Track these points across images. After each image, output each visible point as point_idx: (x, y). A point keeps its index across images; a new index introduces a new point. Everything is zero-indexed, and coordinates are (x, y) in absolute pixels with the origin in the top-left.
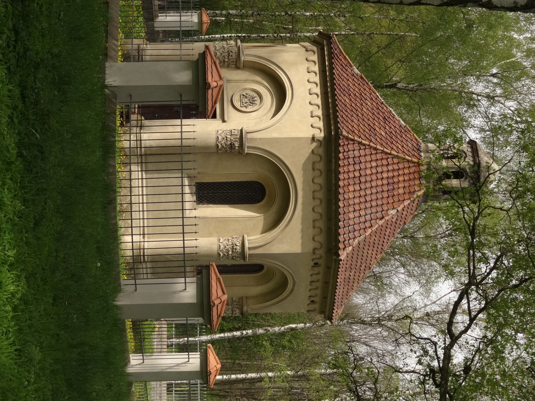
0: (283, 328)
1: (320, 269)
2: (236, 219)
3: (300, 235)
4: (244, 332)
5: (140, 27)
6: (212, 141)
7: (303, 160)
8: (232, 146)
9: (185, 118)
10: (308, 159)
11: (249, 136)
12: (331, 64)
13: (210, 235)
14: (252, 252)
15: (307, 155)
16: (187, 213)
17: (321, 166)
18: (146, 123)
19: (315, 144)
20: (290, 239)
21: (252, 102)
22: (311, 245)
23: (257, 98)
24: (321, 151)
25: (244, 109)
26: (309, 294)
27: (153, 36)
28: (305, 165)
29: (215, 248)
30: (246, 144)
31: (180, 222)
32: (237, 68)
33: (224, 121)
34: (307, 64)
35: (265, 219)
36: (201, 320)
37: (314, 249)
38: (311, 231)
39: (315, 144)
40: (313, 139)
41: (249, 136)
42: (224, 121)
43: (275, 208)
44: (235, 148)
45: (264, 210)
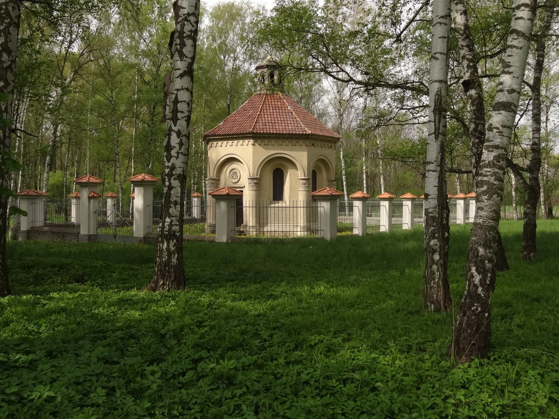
1: (315, 143)
2: (291, 182)
5: (199, 225)
6: (254, 192)
8: (256, 183)
10: (263, 147)
11: (251, 175)
12: (218, 135)
13: (298, 195)
16: (288, 205)
17: (266, 141)
18: (244, 223)
19: (256, 144)
20: (301, 157)
21: (236, 173)
23: (234, 171)
24: (259, 141)
25: (239, 177)
26: (327, 149)
27: (203, 219)
29: (304, 192)
30: (255, 177)
31: (291, 209)
32: (219, 180)
33: (244, 187)
34: (218, 147)
38: (297, 147)
39: (256, 144)
40: (253, 145)
41: (251, 175)
42: (244, 187)
43: (286, 164)
44: (257, 182)
45: (287, 169)
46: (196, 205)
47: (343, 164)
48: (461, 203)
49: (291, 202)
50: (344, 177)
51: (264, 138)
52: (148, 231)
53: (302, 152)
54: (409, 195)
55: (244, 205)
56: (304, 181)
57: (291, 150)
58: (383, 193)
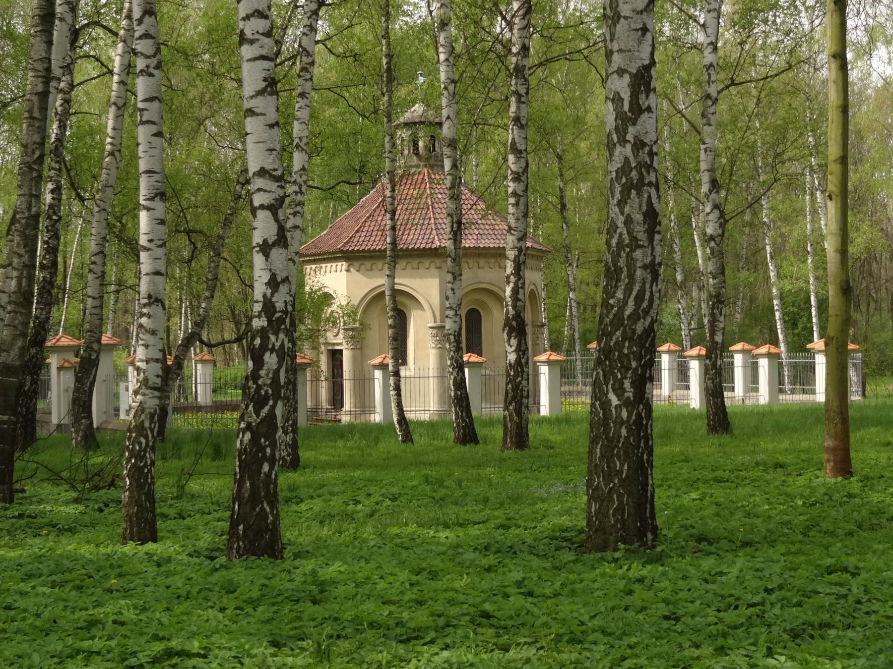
0: (771, 268)
3: (425, 280)
4: (776, 308)
7: (365, 279)
9: (342, 376)
10: (363, 274)
12: (307, 255)
14: (438, 320)
15: (360, 275)
16: (412, 374)
17: (368, 264)
19: (352, 269)
20: (426, 288)
22: (433, 270)
24: (357, 264)
28: (368, 277)
31: (413, 379)
35: (416, 309)
36: (308, 370)
37: (437, 268)
40: (348, 271)
46: (667, 367)
47: (772, 274)
48: (738, 359)
49: (417, 370)
50: (775, 302)
51: (364, 258)
52: (104, 418)
53: (430, 280)
54: (739, 346)
55: (824, 366)
56: (435, 331)
57: (411, 277)
58: (816, 340)
